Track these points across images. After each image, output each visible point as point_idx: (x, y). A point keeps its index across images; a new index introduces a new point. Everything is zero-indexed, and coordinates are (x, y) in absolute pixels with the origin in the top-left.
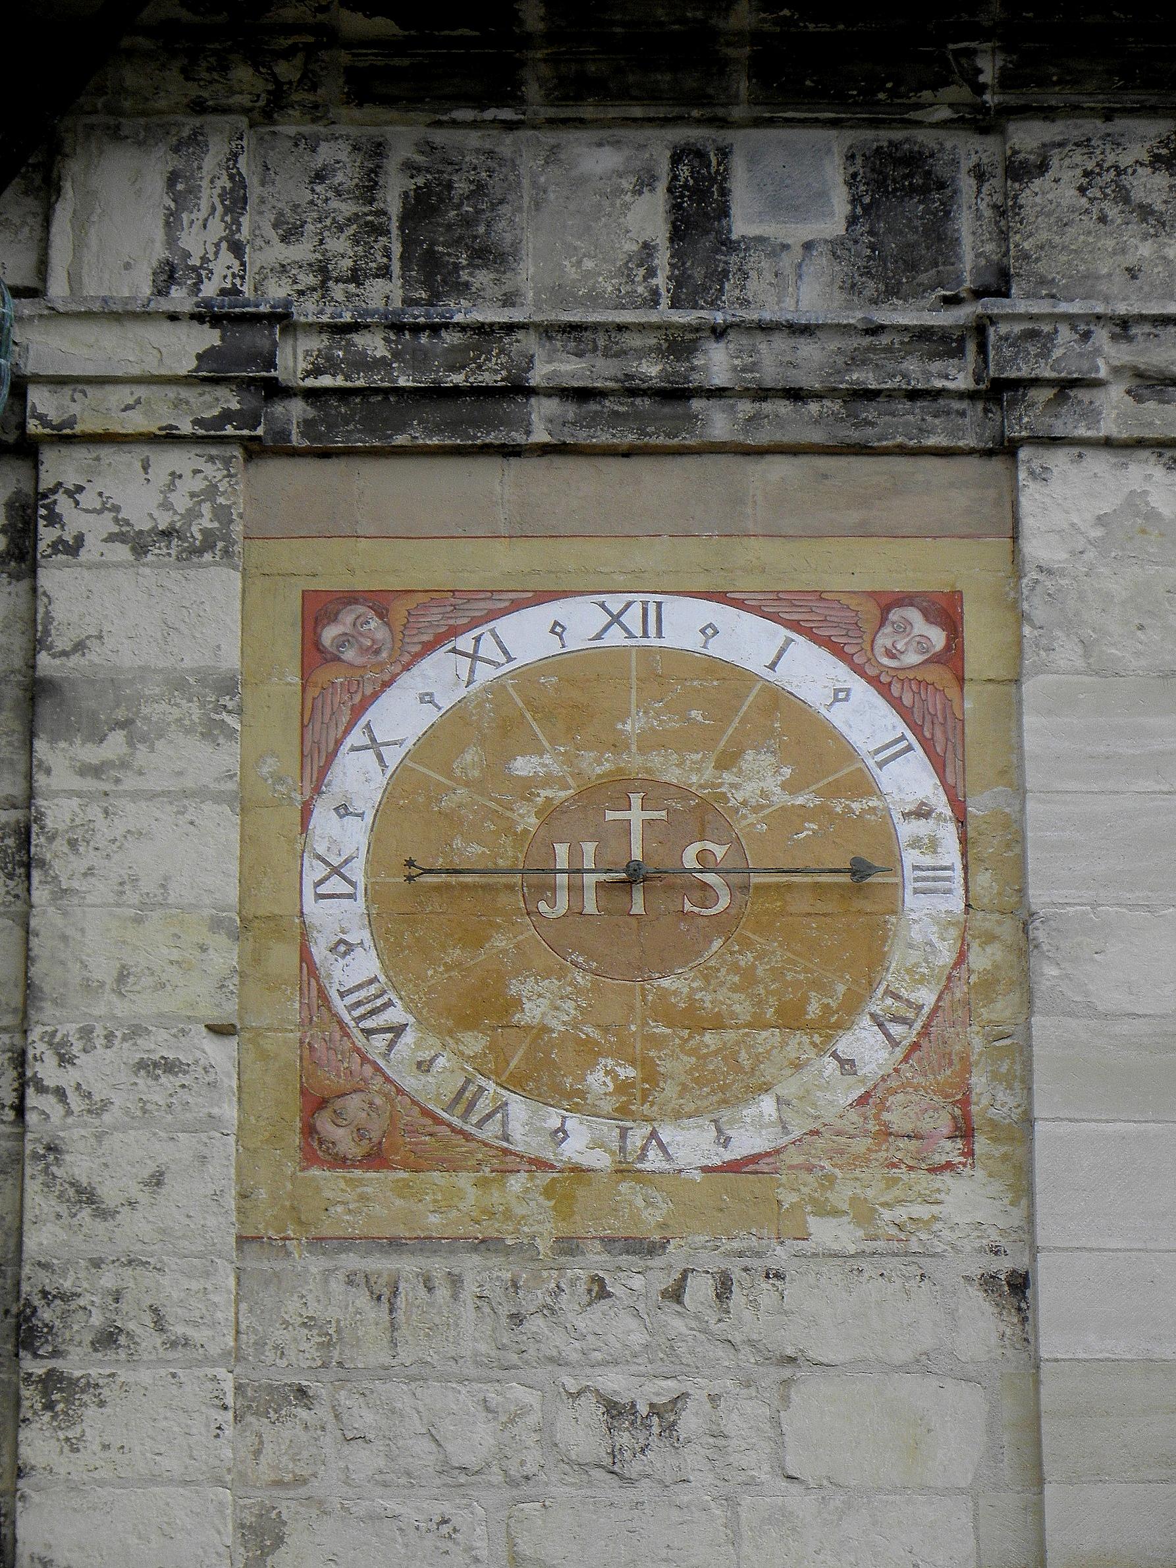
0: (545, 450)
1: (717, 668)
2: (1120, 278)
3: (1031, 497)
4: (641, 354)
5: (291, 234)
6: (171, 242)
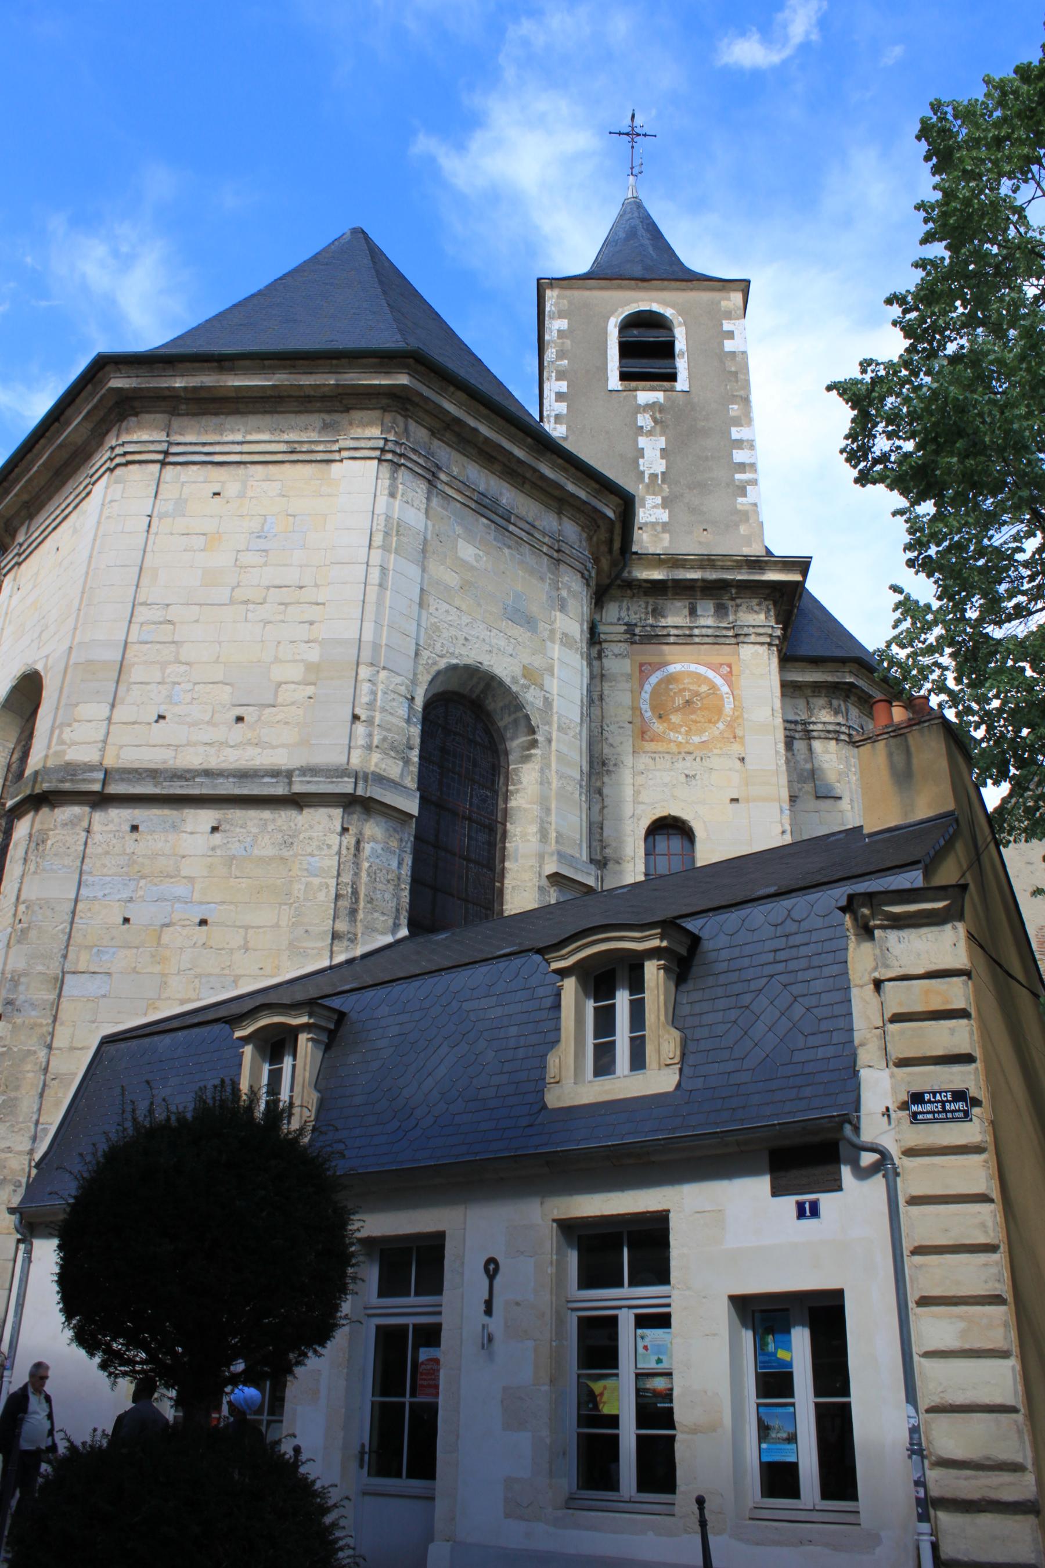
1: (697, 673)
5: (636, 614)
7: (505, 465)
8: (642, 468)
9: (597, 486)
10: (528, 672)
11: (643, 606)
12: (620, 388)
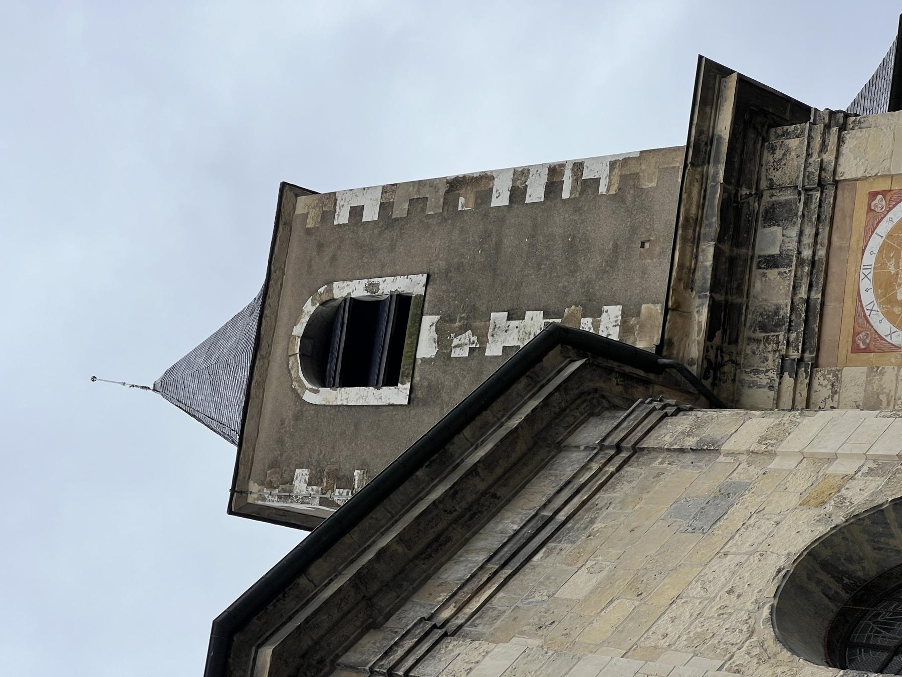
0: (823, 295)
1: (880, 251)
2: (799, 159)
3: (847, 176)
4: (802, 271)
6: (764, 387)
7: (456, 521)
9: (524, 381)
10: (814, 500)
11: (754, 346)
12: (408, 385)
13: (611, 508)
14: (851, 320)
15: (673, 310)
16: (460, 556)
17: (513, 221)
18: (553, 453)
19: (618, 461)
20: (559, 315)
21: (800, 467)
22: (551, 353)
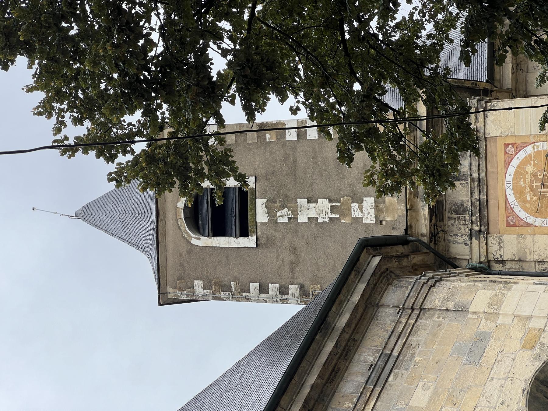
0: (487, 196)
1: (515, 175)
3: (491, 135)
4: (474, 185)
6: (462, 243)
7: (339, 358)
8: (327, 220)
9: (353, 273)
10: (529, 343)
11: (453, 222)
12: (255, 237)
13: (420, 347)
14: (504, 209)
15: (410, 210)
16: (347, 377)
17: (301, 149)
18: (375, 310)
19: (414, 316)
20: (339, 201)
21: (514, 323)
22: (363, 254)
